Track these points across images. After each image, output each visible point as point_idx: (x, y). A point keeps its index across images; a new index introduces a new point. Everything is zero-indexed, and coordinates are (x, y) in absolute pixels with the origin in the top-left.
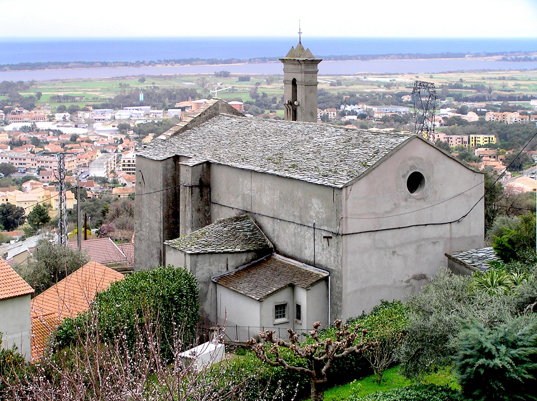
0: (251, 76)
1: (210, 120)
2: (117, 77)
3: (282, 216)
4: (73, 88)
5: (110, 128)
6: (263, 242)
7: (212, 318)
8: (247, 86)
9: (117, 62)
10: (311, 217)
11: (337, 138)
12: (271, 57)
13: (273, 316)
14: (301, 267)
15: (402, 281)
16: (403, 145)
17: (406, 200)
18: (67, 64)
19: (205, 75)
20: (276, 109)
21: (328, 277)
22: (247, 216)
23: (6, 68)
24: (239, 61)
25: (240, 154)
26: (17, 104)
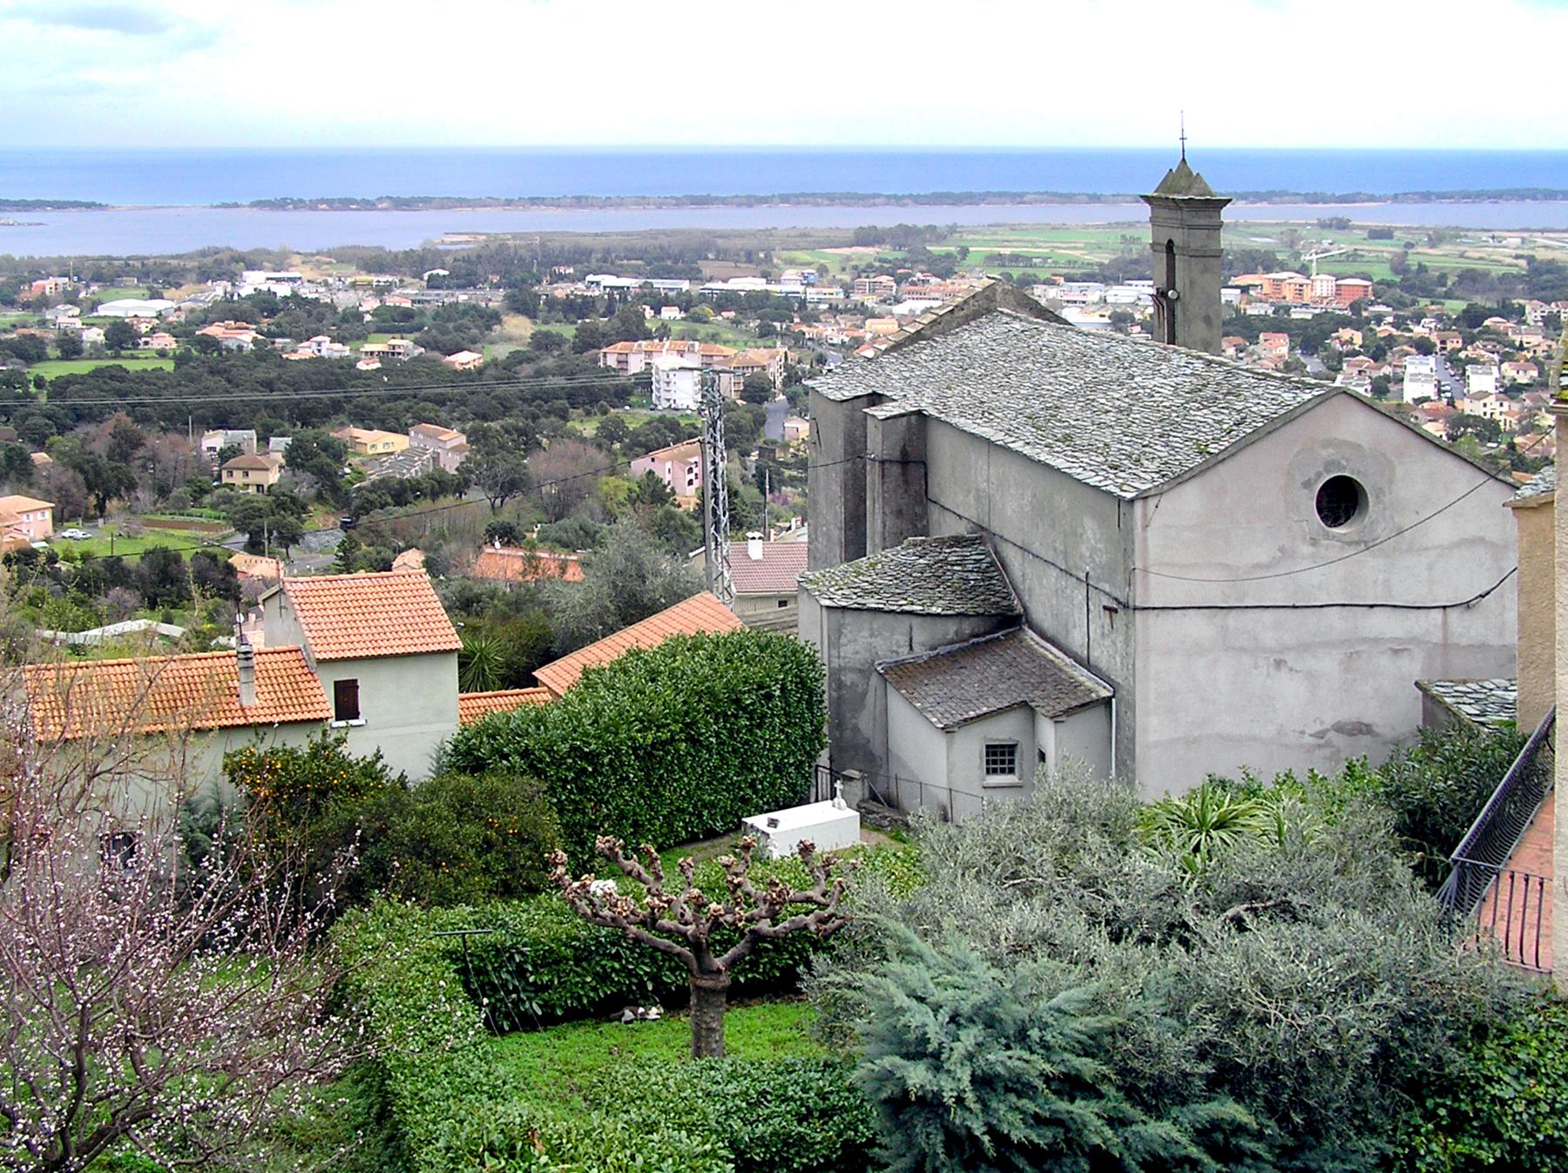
0: (1396, 228)
1: (973, 323)
2: (1117, 223)
3: (1037, 548)
4: (1031, 241)
5: (1095, 318)
6: (1004, 598)
7: (878, 749)
8: (1387, 249)
9: (1119, 195)
10: (1082, 556)
11: (1179, 380)
12: (1443, 190)
13: (980, 767)
14: (1065, 668)
15: (1303, 732)
16: (1304, 409)
17: (1314, 542)
18: (1021, 195)
19: (1299, 225)
20: (1444, 297)
21: (1110, 698)
22: (981, 537)
23: (906, 201)
24: (1372, 199)
25: (985, 399)
26: (923, 267)
